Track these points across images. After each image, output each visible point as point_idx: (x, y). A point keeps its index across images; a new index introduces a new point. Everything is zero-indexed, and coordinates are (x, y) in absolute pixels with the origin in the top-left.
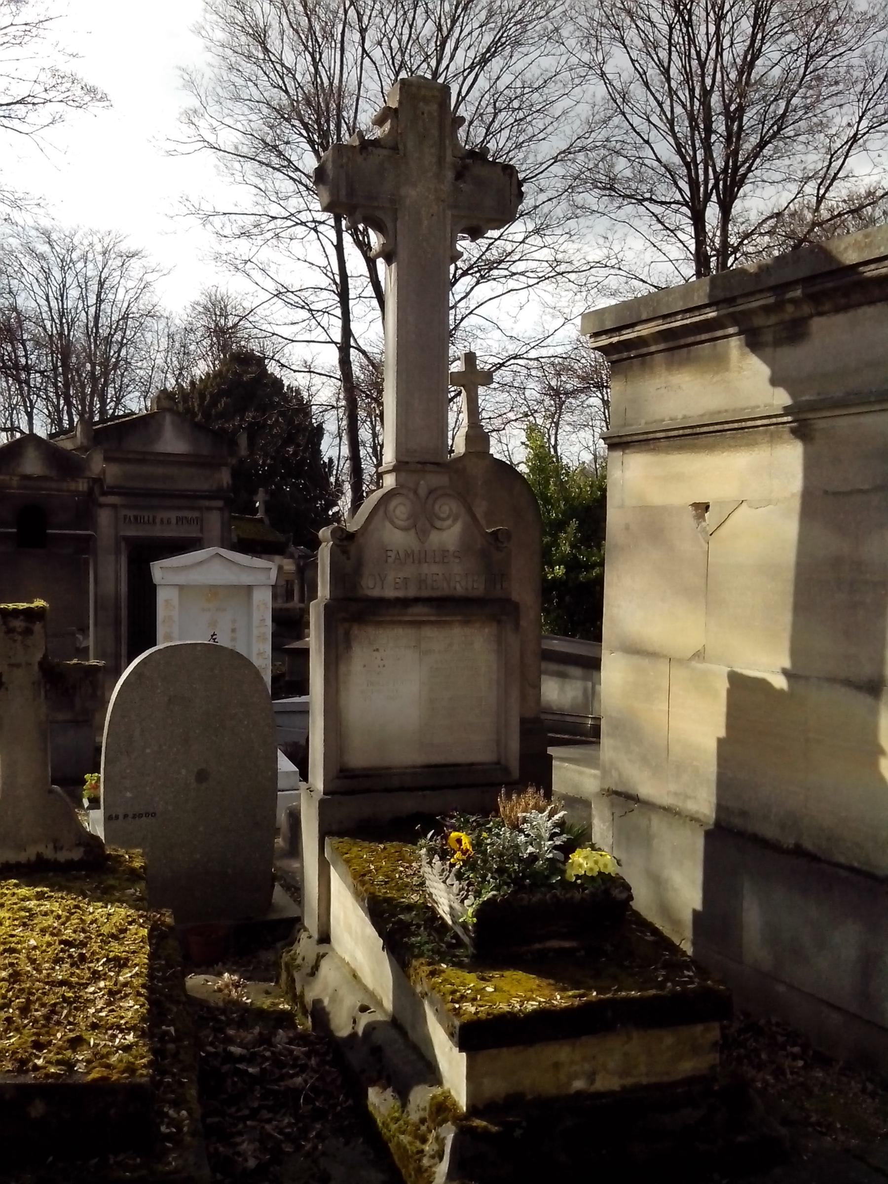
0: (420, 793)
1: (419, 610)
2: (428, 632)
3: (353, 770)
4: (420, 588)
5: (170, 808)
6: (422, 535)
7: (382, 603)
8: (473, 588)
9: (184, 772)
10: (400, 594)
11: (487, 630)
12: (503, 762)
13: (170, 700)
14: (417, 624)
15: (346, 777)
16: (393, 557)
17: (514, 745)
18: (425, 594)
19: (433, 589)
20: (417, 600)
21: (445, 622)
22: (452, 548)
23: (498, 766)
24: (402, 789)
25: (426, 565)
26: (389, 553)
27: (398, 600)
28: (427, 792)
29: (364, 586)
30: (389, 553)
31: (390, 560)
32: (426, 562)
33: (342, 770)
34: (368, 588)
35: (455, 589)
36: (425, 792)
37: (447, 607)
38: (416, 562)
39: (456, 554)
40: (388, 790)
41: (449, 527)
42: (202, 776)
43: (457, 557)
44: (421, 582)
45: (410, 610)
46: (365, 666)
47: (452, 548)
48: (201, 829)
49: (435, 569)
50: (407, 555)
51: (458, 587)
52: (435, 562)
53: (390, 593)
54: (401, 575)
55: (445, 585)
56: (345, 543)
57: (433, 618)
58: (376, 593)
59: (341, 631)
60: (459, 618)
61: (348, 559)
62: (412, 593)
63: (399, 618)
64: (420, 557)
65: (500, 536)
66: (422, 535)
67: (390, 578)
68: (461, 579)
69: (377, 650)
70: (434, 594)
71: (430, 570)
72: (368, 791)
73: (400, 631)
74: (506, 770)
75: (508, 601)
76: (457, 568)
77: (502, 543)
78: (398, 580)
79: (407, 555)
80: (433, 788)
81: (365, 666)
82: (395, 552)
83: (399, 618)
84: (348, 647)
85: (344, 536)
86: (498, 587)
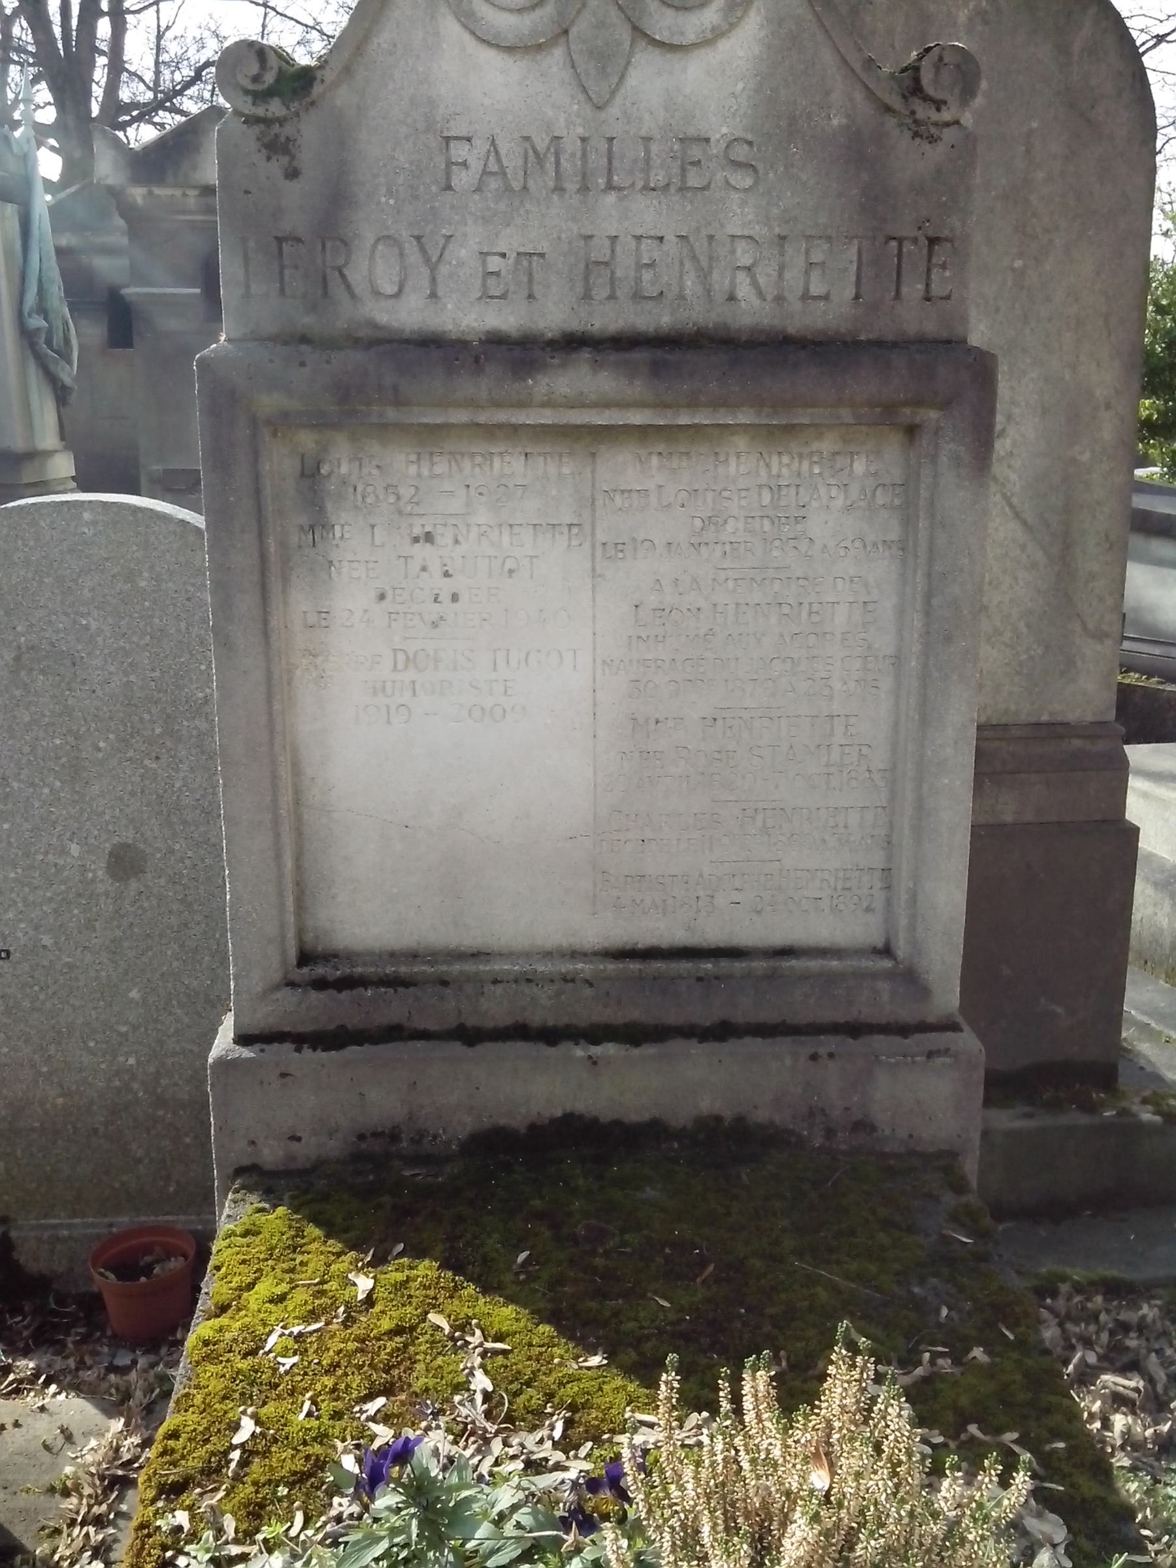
0: (579, 1052)
1: (578, 379)
2: (623, 468)
3: (350, 957)
4: (587, 296)
5: (47, 940)
6: (598, 79)
7: (436, 350)
8: (806, 296)
9: (75, 849)
10: (506, 319)
11: (859, 466)
12: (902, 949)
13: (17, 659)
14: (590, 438)
15: (320, 984)
16: (476, 166)
17: (947, 897)
18: (607, 319)
19: (638, 296)
20: (572, 343)
21: (695, 432)
22: (720, 130)
23: (887, 964)
24: (520, 1032)
25: (611, 198)
26: (459, 151)
27: (496, 341)
28: (610, 1049)
29: (360, 288)
30: (459, 151)
31: (463, 179)
32: (610, 187)
33: (305, 958)
34: (377, 293)
35: (732, 298)
36: (596, 1050)
37: (698, 370)
38: (571, 186)
39: (741, 153)
40: (469, 1036)
41: (708, 41)
42: (125, 863)
43: (737, 165)
44: (592, 270)
45: (541, 385)
46: (382, 597)
47: (720, 130)
48: (134, 994)
49: (648, 215)
50: (534, 157)
51: (744, 290)
52: (648, 189)
53: (467, 315)
54: (510, 241)
55: (690, 283)
56: (275, 108)
57: (637, 418)
58: (410, 314)
59: (280, 463)
60: (744, 417)
61: (293, 174)
62: (554, 314)
63: (502, 416)
64: (593, 170)
65: (926, 77)
66: (598, 79)
67: (463, 253)
68: (759, 260)
69: (429, 538)
70: (663, 319)
71: (633, 219)
72: (394, 1033)
73: (512, 465)
74: (910, 979)
75: (951, 345)
76: (740, 215)
77: (939, 105)
78: (494, 263)
79: (534, 157)
80: (633, 1035)
81: (382, 597)
82: (481, 145)
83: (502, 416)
84: (318, 524)
85: (269, 78)
86: (913, 289)
